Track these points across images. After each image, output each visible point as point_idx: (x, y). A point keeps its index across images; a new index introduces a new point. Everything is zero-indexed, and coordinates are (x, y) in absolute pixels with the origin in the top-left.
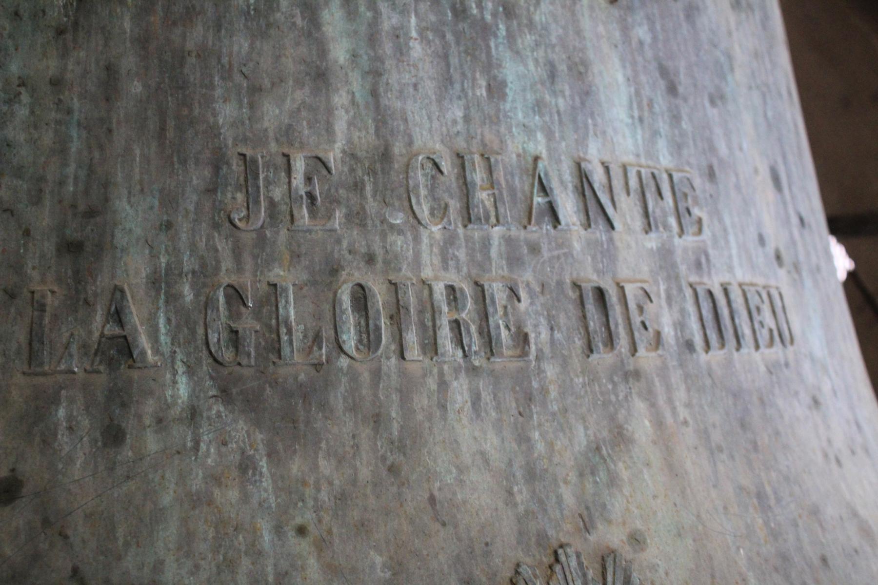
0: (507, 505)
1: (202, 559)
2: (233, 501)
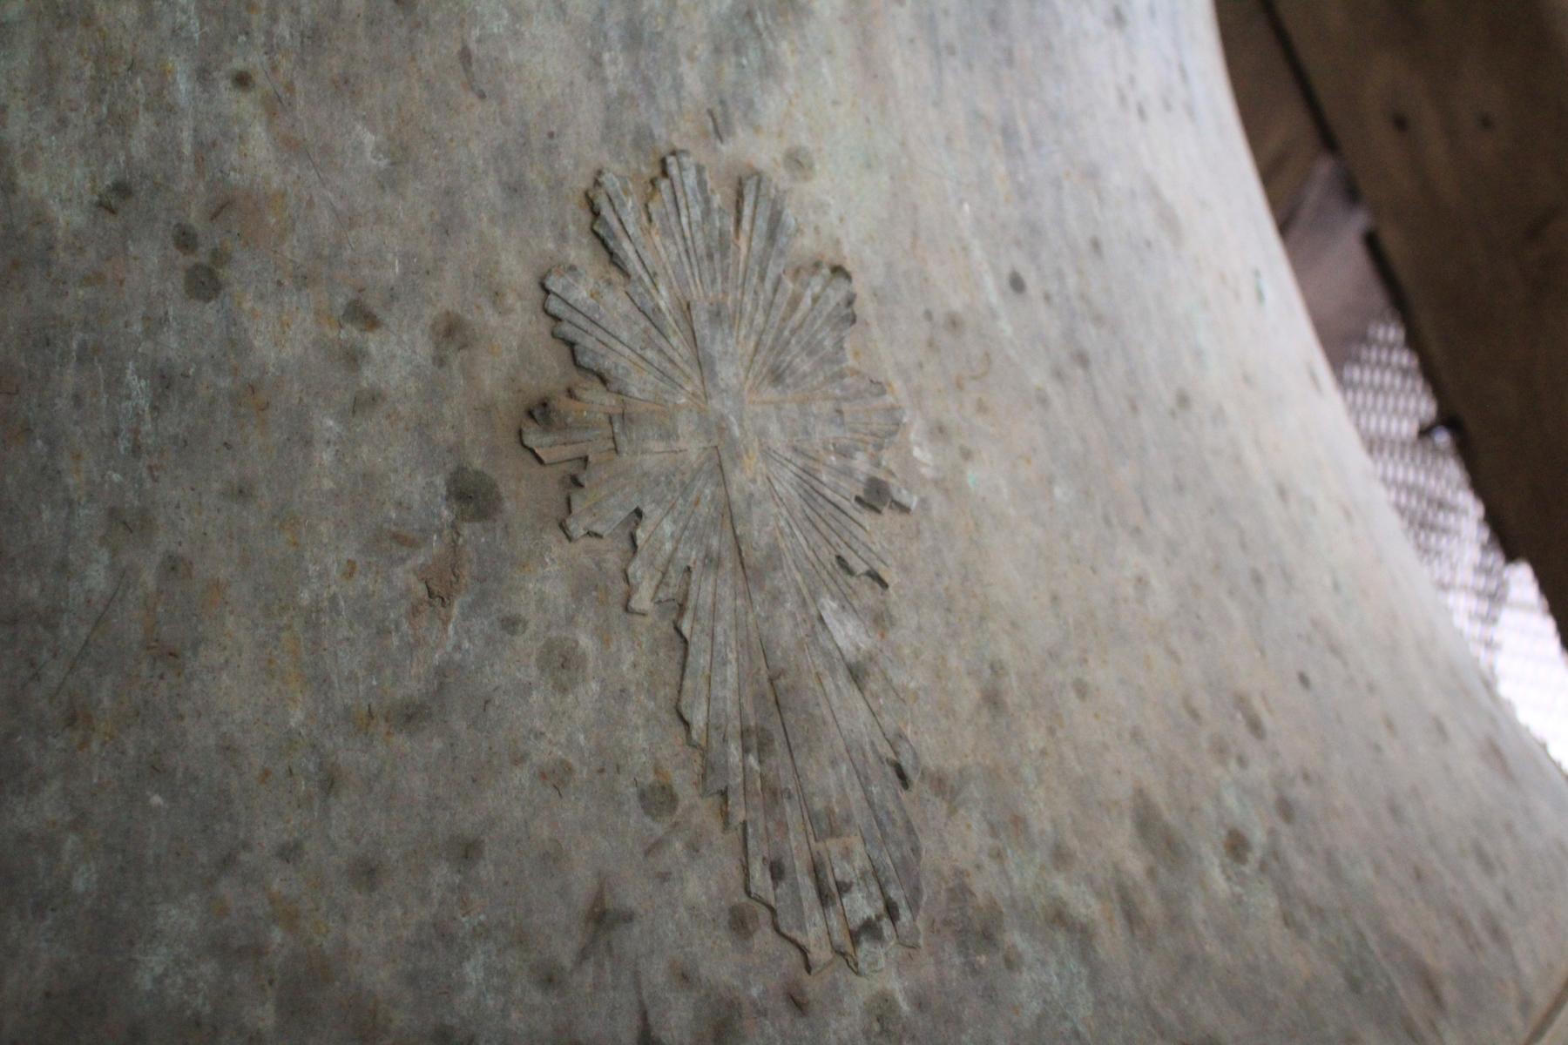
0: (590, 79)
1: (72, 110)
2: (128, 23)
